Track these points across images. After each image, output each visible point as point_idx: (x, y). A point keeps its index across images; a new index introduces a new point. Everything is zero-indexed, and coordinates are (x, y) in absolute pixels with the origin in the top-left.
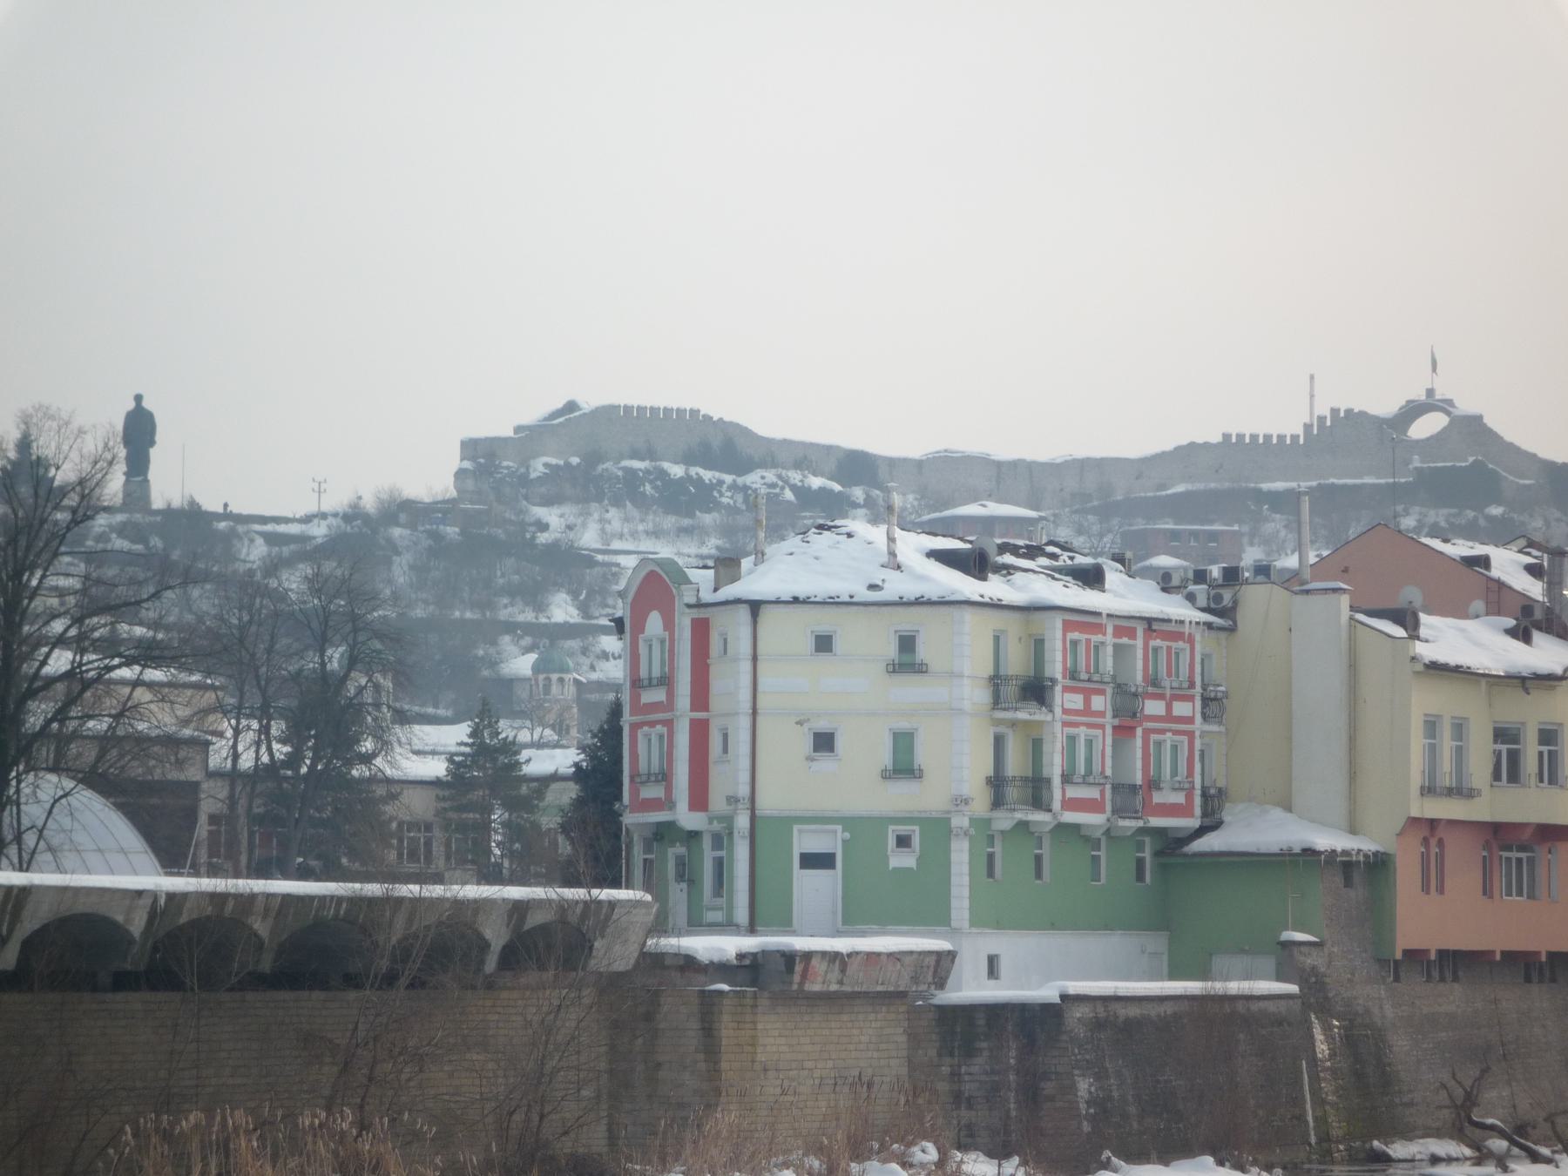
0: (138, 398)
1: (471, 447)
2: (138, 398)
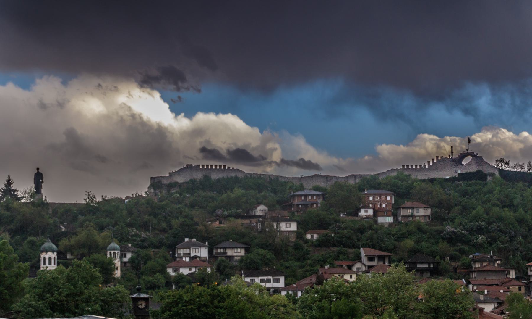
0: (38, 169)
2: (38, 169)
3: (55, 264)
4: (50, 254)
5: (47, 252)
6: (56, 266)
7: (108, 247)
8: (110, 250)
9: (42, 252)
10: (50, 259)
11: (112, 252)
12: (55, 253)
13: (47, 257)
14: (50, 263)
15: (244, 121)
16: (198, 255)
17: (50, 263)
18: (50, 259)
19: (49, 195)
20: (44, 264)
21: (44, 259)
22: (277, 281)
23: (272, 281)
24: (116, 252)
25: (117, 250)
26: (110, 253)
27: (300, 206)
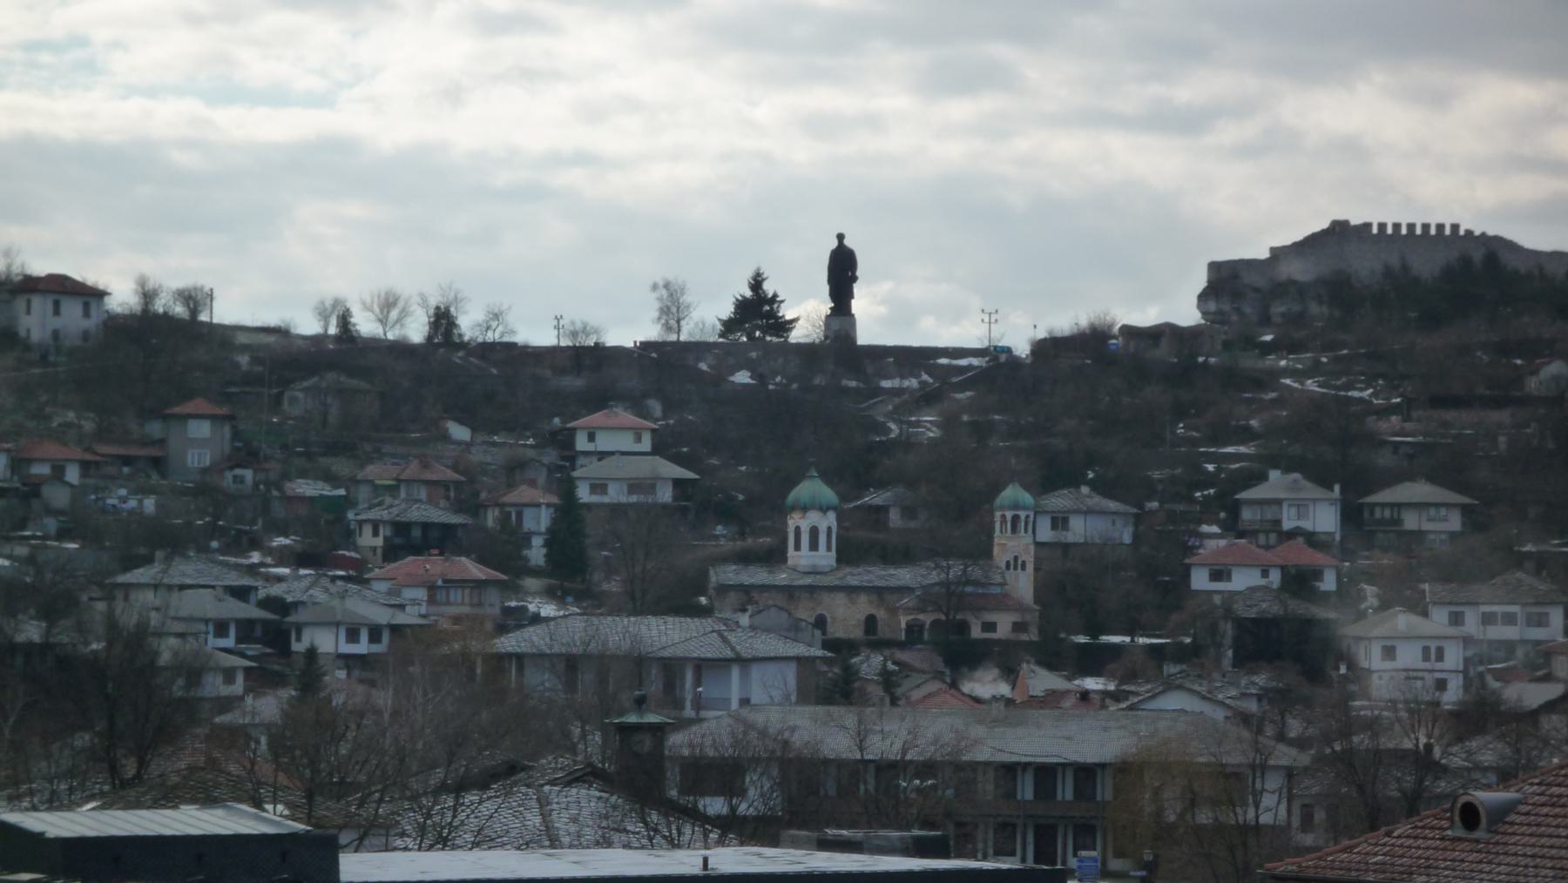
0: (841, 237)
1: (1215, 267)
2: (841, 237)
3: (829, 549)
4: (814, 518)
5: (805, 509)
6: (833, 553)
7: (998, 502)
8: (1002, 508)
9: (793, 508)
10: (814, 532)
11: (1009, 515)
12: (832, 516)
13: (805, 526)
14: (814, 546)
15: (526, 347)
16: (1307, 525)
17: (814, 546)
18: (814, 532)
19: (874, 321)
20: (797, 547)
21: (798, 530)
22: (1541, 621)
23: (1520, 618)
24: (1023, 514)
25: (1025, 508)
26: (1003, 516)
27: (847, 524)
